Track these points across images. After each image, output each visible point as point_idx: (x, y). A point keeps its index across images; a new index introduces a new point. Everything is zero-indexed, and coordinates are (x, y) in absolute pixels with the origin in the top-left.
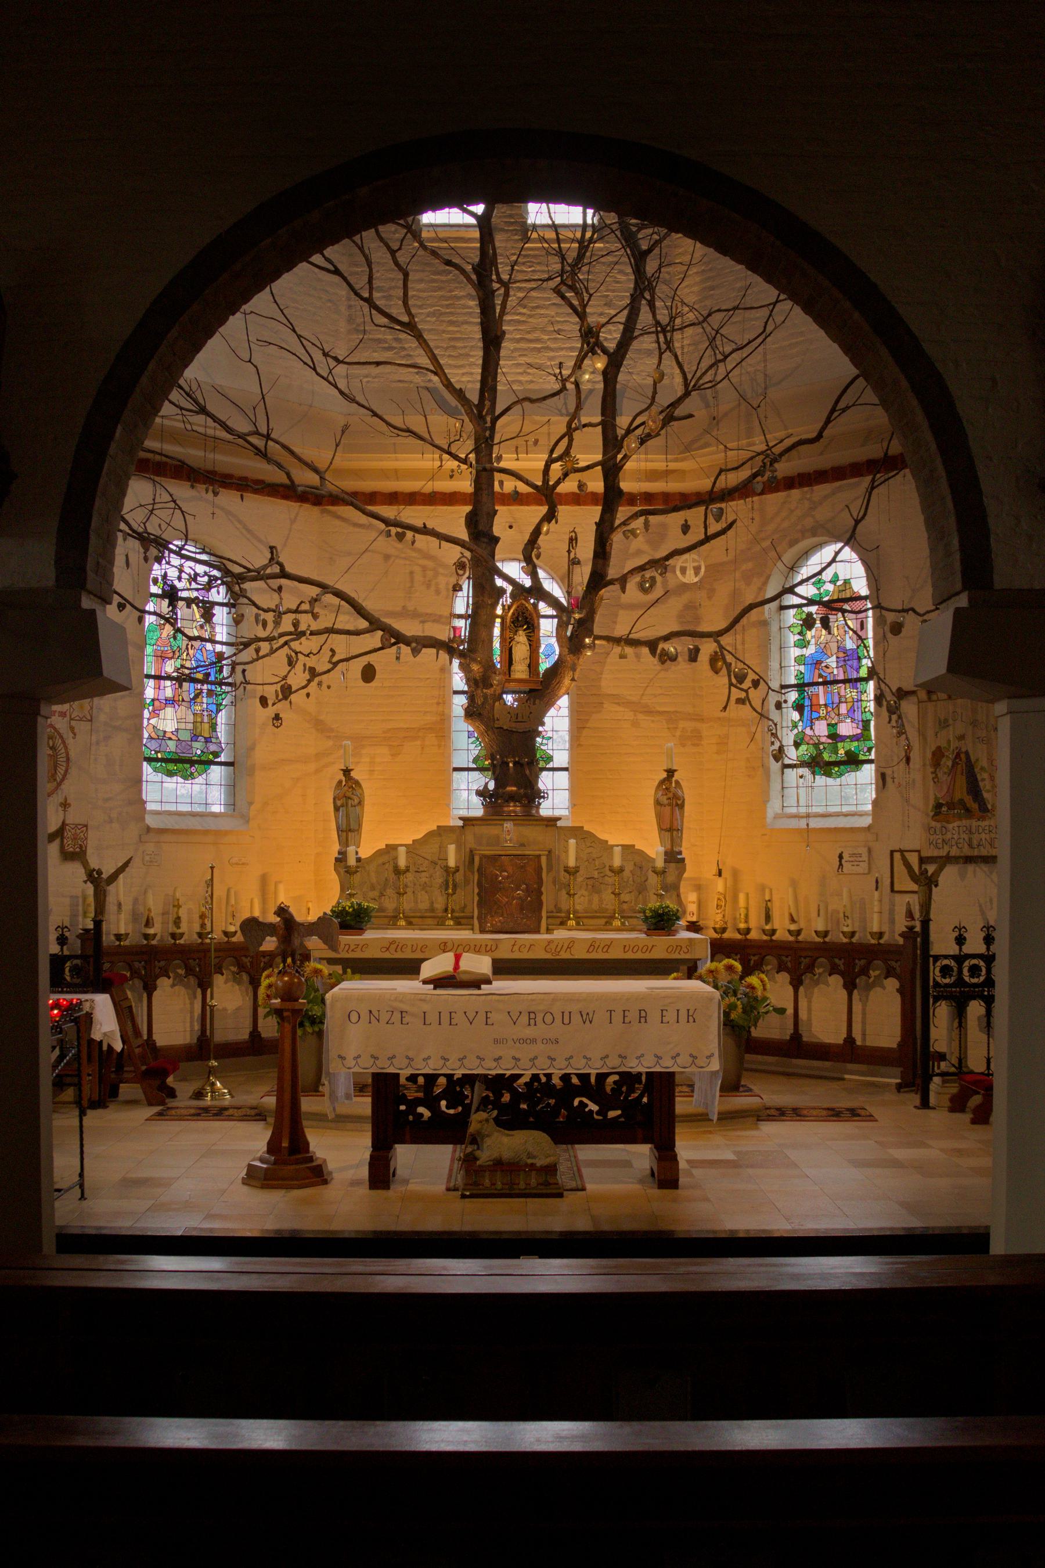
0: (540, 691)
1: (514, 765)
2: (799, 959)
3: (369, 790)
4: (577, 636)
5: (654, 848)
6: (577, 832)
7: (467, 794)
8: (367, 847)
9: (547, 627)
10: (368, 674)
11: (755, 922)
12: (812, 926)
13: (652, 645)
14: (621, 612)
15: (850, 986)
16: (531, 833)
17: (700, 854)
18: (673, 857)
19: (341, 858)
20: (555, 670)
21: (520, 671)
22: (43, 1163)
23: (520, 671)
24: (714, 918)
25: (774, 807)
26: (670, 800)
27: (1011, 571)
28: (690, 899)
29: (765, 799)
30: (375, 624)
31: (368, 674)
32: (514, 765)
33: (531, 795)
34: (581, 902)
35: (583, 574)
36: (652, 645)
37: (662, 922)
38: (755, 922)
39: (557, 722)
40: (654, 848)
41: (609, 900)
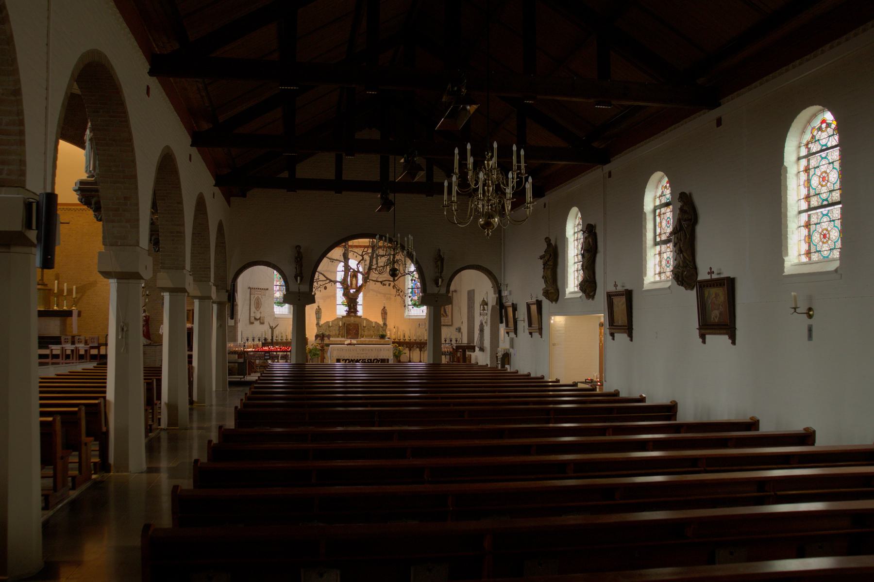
0: (359, 290)
1: (352, 303)
2: (410, 345)
3: (323, 310)
4: (366, 280)
5: (381, 322)
6: (366, 319)
7: (342, 310)
8: (322, 322)
9: (360, 277)
10: (325, 288)
11: (402, 337)
12: (413, 338)
13: (381, 282)
14: (374, 275)
15: (421, 351)
16: (356, 319)
17: (391, 324)
18: (385, 324)
19: (318, 324)
20: (361, 287)
21: (354, 286)
22: (783, 199)
23: (354, 286)
24: (393, 337)
25: (406, 313)
26: (384, 313)
27: (429, 291)
28: (388, 333)
29: (404, 312)
30: (327, 279)
31: (325, 288)
32: (352, 303)
33: (356, 311)
34: (366, 333)
35: (367, 267)
36: (381, 282)
37: (383, 337)
38: (402, 337)
39: (360, 299)
40: (381, 322)
41: (372, 332)
